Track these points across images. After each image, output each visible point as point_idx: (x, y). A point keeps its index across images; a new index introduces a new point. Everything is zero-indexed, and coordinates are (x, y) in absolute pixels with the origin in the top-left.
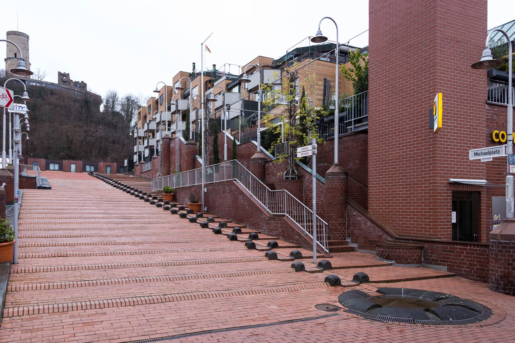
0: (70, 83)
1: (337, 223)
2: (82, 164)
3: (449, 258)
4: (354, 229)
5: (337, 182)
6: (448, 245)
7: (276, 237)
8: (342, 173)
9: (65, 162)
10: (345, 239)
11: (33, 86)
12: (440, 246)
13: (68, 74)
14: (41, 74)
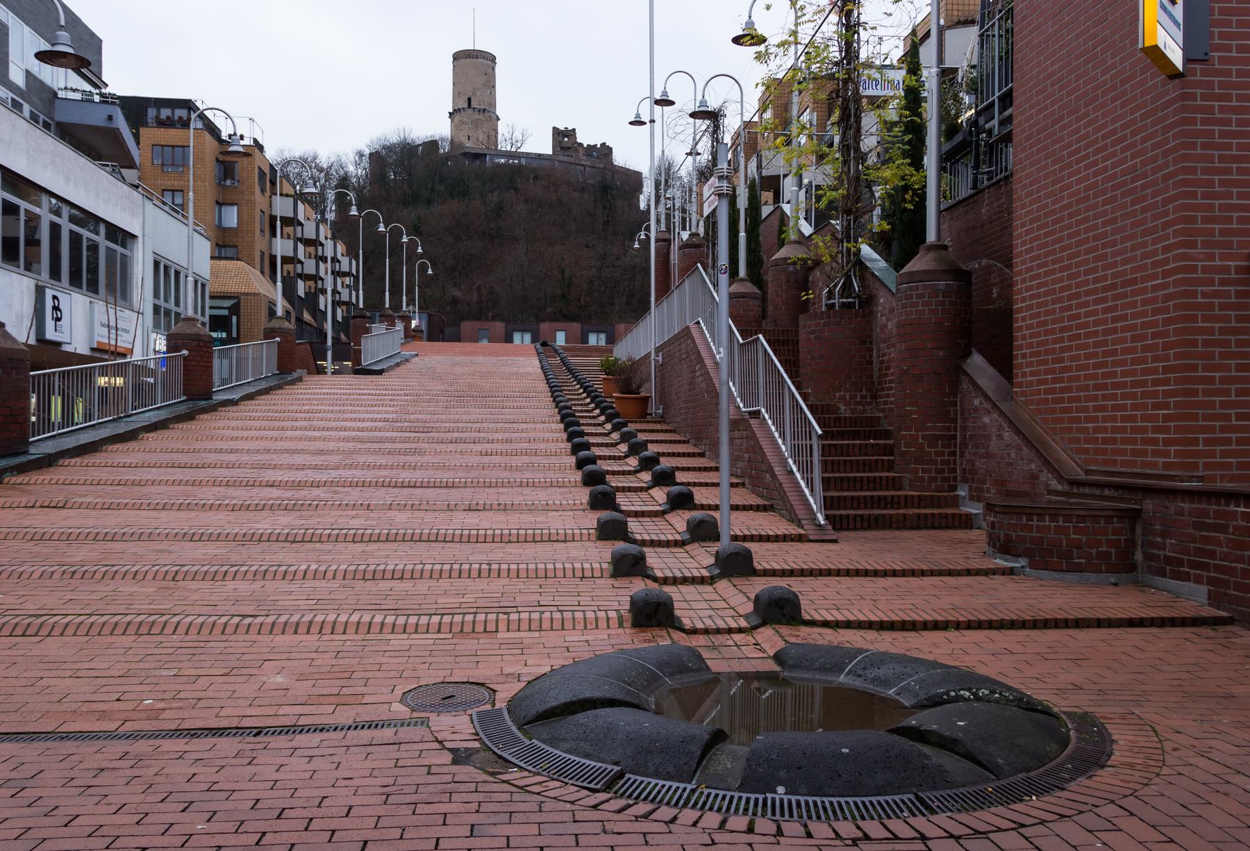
0: (576, 150)
1: (924, 437)
2: (579, 329)
3: (1212, 554)
4: (975, 454)
5: (924, 304)
6: (1238, 506)
8: (943, 271)
9: (544, 327)
10: (954, 488)
11: (499, 165)
12: (1186, 506)
13: (574, 130)
14: (517, 135)
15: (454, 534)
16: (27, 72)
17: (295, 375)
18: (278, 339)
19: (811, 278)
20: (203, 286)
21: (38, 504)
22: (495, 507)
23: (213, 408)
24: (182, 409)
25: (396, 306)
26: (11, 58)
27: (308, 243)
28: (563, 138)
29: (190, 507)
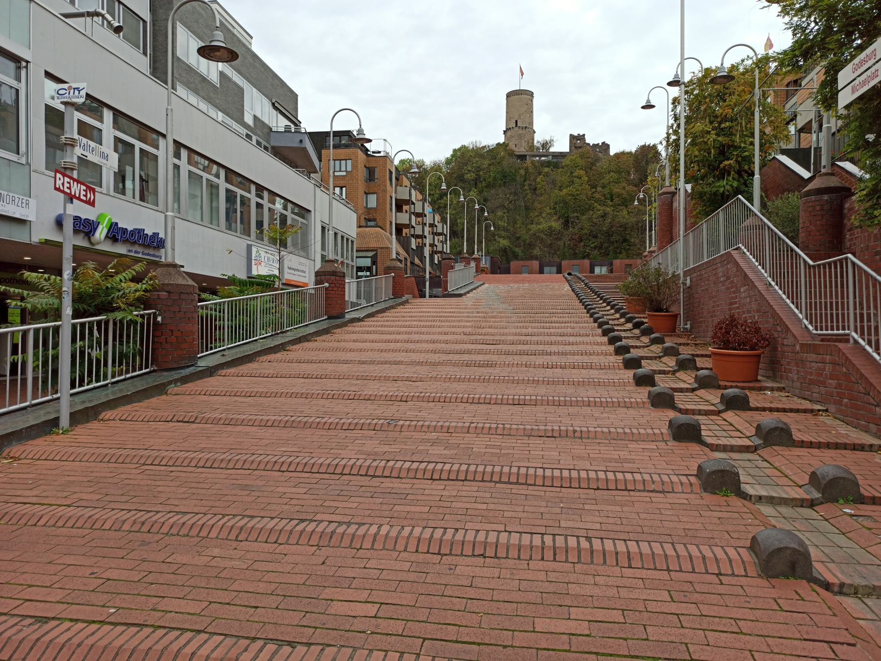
7: (817, 407)
15: (508, 398)
16: (255, 117)
17: (404, 299)
18: (393, 274)
19: (847, 205)
20: (352, 242)
21: (175, 419)
22: (570, 434)
23: (345, 324)
24: (325, 325)
25: (471, 252)
26: (245, 108)
27: (418, 215)
28: (577, 141)
29: (294, 425)
